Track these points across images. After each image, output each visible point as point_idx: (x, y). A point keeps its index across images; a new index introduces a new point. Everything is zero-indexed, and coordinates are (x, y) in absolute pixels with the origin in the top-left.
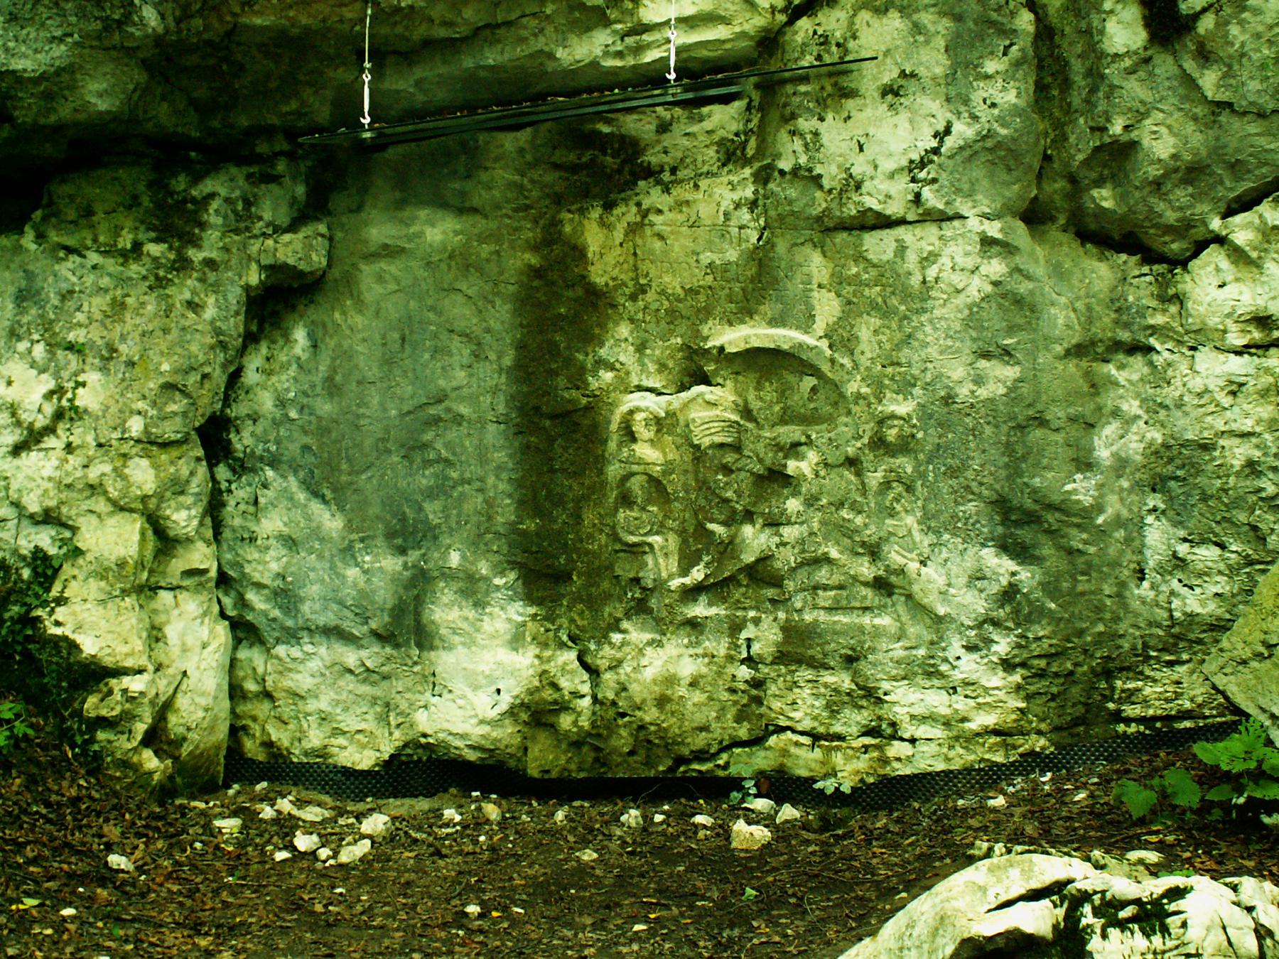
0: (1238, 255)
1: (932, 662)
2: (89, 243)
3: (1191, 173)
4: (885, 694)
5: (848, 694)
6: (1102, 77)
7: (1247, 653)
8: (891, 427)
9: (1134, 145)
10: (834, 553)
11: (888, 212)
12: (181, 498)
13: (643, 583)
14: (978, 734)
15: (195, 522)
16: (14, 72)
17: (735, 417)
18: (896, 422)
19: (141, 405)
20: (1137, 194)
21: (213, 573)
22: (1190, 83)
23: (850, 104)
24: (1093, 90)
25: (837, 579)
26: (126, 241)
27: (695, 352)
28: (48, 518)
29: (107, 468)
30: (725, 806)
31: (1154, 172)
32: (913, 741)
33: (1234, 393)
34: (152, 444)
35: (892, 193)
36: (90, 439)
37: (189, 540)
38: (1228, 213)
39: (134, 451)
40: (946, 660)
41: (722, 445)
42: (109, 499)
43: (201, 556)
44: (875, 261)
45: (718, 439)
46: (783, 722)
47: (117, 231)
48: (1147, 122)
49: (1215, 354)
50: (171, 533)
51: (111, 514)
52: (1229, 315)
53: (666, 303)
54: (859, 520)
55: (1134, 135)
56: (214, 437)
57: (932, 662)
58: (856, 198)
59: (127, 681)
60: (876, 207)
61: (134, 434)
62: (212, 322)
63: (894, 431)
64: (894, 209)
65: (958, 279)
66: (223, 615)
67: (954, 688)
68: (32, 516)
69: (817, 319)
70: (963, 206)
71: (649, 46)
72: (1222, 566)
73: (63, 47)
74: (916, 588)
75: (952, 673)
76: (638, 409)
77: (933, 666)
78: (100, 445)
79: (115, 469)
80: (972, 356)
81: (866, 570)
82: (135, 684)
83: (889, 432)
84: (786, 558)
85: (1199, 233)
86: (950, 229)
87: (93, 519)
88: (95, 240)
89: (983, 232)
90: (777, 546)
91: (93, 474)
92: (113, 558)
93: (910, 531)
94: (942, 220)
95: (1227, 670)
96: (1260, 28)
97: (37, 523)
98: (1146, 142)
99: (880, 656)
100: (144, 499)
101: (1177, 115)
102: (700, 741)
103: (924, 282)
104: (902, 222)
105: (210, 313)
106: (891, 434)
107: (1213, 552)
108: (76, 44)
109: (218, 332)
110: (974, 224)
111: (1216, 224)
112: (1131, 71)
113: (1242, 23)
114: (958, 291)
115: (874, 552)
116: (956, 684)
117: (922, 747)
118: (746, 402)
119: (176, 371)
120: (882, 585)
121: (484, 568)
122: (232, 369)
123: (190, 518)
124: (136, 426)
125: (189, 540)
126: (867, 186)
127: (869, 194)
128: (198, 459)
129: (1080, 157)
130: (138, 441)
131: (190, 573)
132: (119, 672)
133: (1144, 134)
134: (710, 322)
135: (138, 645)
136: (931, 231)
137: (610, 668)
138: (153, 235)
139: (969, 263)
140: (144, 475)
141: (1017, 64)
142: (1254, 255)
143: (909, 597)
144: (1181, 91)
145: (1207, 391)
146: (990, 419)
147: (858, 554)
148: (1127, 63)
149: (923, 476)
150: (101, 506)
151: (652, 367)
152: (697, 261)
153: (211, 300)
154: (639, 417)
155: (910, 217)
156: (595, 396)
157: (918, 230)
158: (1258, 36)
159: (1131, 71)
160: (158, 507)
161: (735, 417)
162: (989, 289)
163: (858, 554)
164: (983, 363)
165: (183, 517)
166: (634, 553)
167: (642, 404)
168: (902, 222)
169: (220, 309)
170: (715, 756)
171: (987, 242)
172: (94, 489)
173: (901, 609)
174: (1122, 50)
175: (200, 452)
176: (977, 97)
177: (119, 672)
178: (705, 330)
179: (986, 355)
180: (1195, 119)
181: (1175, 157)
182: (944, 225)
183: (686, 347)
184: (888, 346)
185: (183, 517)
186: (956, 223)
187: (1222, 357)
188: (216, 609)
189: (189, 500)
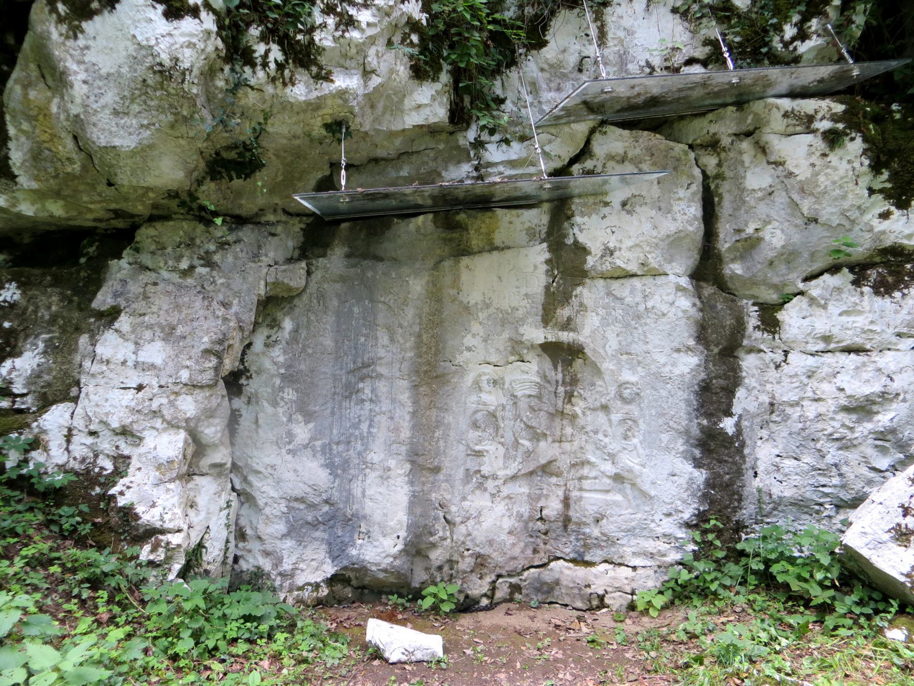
0: (813, 301)
2: (162, 264)
3: (789, 256)
6: (744, 202)
9: (760, 240)
10: (593, 459)
11: (628, 268)
12: (211, 420)
14: (672, 565)
15: (219, 435)
16: (114, 147)
17: (538, 380)
19: (188, 363)
20: (759, 266)
21: (229, 465)
22: (795, 205)
23: (605, 210)
24: (737, 209)
25: (593, 474)
26: (184, 265)
28: (124, 432)
29: (164, 401)
30: (83, 260)
31: (771, 254)
32: (634, 568)
33: (809, 377)
34: (192, 386)
36: (155, 383)
37: (215, 446)
38: (807, 279)
39: (183, 390)
41: (530, 396)
42: (164, 420)
43: (221, 456)
45: (527, 392)
46: (559, 554)
47: (179, 259)
48: (769, 227)
49: (801, 355)
50: (204, 442)
51: (164, 430)
52: (809, 334)
54: (606, 440)
55: (761, 234)
56: (234, 382)
58: (610, 259)
59: (169, 537)
60: (623, 266)
61: (184, 380)
62: (236, 314)
63: (628, 391)
64: (633, 267)
65: (664, 308)
66: (233, 489)
68: (114, 430)
70: (667, 268)
71: (490, 175)
72: (798, 470)
73: (148, 132)
74: (638, 481)
76: (485, 374)
78: (161, 387)
79: (170, 402)
82: (175, 539)
84: (564, 462)
85: (790, 290)
86: (660, 280)
87: (155, 433)
88: (166, 263)
91: (155, 405)
92: (165, 458)
95: (871, 546)
96: (836, 178)
97: (117, 434)
98: (767, 238)
100: (187, 420)
101: (786, 224)
102: (511, 566)
105: (235, 308)
106: (626, 393)
107: (794, 463)
108: (157, 130)
109: (239, 320)
111: (801, 286)
112: (761, 199)
113: (826, 175)
114: (664, 315)
117: (640, 571)
119: (213, 343)
120: (618, 478)
121: (392, 463)
122: (247, 342)
123: (216, 432)
124: (185, 375)
125: (215, 446)
126: (617, 254)
128: (223, 396)
129: (727, 245)
130: (186, 385)
131: (214, 466)
132: (163, 532)
133: (766, 234)
135: (178, 511)
136: (648, 280)
138: (202, 262)
139: (671, 298)
140: (188, 405)
141: (694, 194)
142: (823, 302)
143: (633, 485)
144: (789, 211)
145: (796, 375)
148: (760, 194)
150: (158, 423)
153: (235, 302)
154: (484, 378)
158: (834, 183)
159: (761, 199)
160: (197, 426)
161: (538, 380)
164: (675, 355)
165: (212, 431)
167: (486, 371)
169: (243, 309)
170: (519, 574)
172: (155, 414)
174: (756, 188)
175: (225, 392)
176: (676, 208)
177: (163, 532)
178: (521, 331)
179: (678, 351)
180: (796, 226)
181: (783, 247)
183: (511, 339)
185: (212, 431)
186: (663, 277)
187: (805, 356)
188: (230, 486)
189: (217, 421)
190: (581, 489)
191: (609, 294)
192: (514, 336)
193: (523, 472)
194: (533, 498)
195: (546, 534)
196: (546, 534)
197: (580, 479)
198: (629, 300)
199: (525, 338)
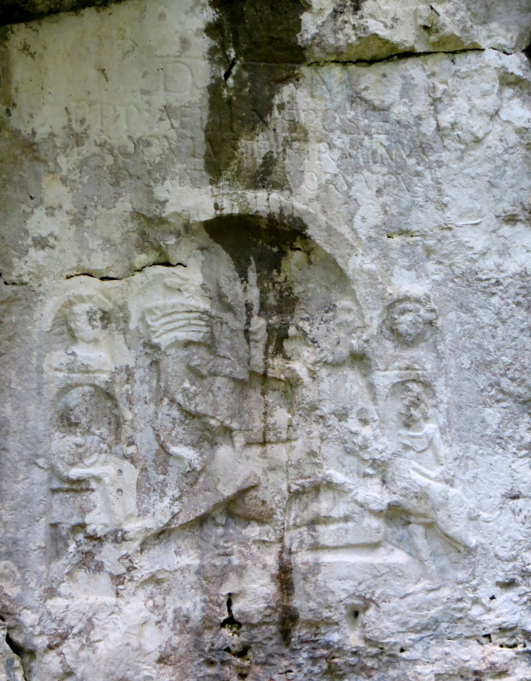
1: (461, 605)
4: (402, 650)
5: (355, 653)
7: (287, 542)
8: (403, 312)
10: (338, 477)
13: (90, 530)
17: (204, 305)
18: (409, 306)
27: (150, 221)
35: (399, 15)
40: (476, 601)
41: (188, 344)
44: (377, 103)
45: (182, 335)
53: (110, 160)
54: (366, 431)
57: (461, 605)
58: (353, 20)
60: (384, 33)
63: (408, 317)
64: (405, 36)
67: (488, 636)
69: (307, 175)
70: (480, 35)
75: (486, 617)
76: (81, 300)
77: (461, 610)
80: (495, 221)
81: (374, 494)
83: (403, 318)
84: (274, 489)
86: (466, 63)
89: (503, 67)
90: (265, 472)
93: (431, 443)
94: (454, 53)
99: (394, 603)
103: (438, 128)
104: (409, 54)
110: (491, 56)
114: (478, 141)
115: (381, 469)
116: (489, 631)
118: (219, 287)
120: (396, 515)
127: (372, 16)
134: (168, 183)
137: (50, 647)
143: (430, 526)
146: (520, 299)
147: (366, 475)
149: (443, 371)
151: (95, 243)
152: (148, 103)
154: (80, 309)
155: (419, 48)
156: (23, 284)
157: (431, 62)
161: (204, 305)
162: (513, 138)
163: (366, 475)
164: (506, 230)
166: (76, 491)
167: (84, 292)
168: (409, 54)
171: (507, 80)
173: (420, 541)
178: (160, 193)
182: (457, 57)
183: (137, 215)
184: (394, 210)
186: (471, 57)
190: (316, 547)
191: (355, 98)
192: (144, 207)
193: (182, 519)
194: (208, 578)
195: (242, 654)
196: (242, 654)
197: (314, 523)
198: (399, 111)
199: (169, 209)
